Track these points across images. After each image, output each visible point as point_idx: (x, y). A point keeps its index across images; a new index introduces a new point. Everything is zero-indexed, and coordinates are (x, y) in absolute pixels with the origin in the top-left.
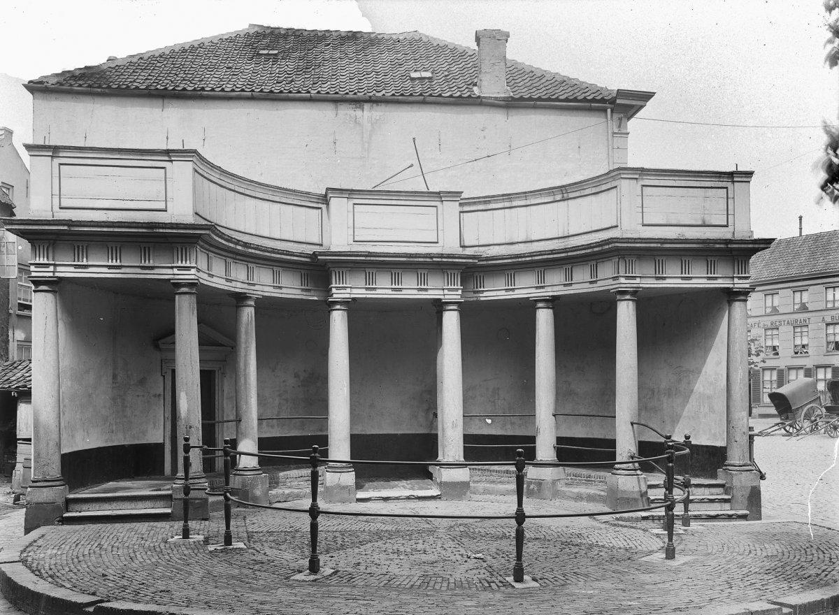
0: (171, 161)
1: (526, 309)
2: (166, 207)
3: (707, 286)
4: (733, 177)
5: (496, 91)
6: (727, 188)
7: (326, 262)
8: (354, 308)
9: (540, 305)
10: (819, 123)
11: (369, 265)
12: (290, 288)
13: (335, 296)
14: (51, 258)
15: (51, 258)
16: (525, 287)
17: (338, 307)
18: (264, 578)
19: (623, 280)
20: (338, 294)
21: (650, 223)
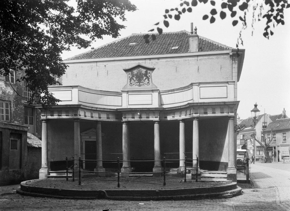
0: (73, 89)
1: (177, 123)
2: (72, 100)
3: (91, 119)
4: (228, 83)
5: (108, 65)
6: (227, 86)
7: (120, 112)
8: (128, 123)
9: (180, 121)
10: (155, 67)
11: (133, 112)
12: (112, 119)
13: (123, 120)
14: (45, 114)
15: (45, 114)
16: (177, 117)
17: (156, 123)
18: (222, 184)
19: (194, 115)
20: (124, 120)
21: (214, 97)
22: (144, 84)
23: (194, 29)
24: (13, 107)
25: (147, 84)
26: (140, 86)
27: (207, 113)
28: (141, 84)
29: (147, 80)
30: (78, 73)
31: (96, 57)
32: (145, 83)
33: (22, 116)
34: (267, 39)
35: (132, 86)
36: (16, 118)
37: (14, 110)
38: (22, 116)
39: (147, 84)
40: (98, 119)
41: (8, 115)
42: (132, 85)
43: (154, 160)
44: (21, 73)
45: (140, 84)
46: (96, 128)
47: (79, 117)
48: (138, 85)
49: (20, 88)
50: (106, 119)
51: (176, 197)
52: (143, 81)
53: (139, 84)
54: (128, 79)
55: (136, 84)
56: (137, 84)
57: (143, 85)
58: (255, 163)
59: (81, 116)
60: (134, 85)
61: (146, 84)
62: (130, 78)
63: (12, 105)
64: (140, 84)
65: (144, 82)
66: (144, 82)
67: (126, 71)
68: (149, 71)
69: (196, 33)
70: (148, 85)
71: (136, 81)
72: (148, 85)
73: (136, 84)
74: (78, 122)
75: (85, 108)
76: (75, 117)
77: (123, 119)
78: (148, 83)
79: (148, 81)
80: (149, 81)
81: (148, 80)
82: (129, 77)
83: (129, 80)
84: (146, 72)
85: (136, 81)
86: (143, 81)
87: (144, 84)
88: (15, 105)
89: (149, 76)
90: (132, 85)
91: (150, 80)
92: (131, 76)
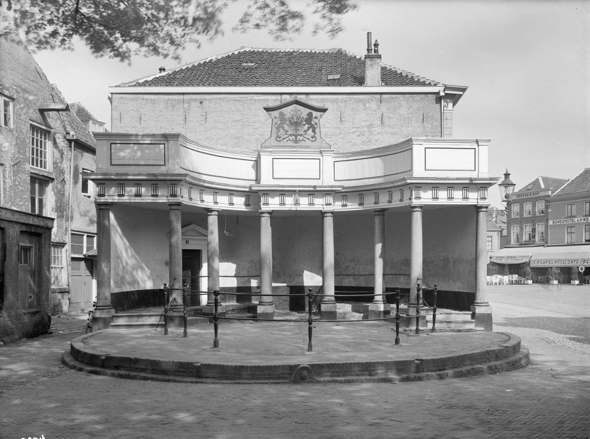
2: (428, 170)
12: (239, 204)
22: (304, 138)
23: (373, 43)
24: (9, 176)
25: (311, 139)
26: (296, 143)
27: (141, 195)
28: (298, 139)
29: (310, 131)
30: (145, 114)
31: (181, 84)
32: (308, 137)
33: (25, 196)
34: (68, 52)
35: (280, 141)
36: (15, 199)
37: (10, 184)
38: (25, 196)
39: (311, 139)
40: (294, 208)
41: (39, 196)
42: (281, 139)
43: (373, 293)
44: (24, 107)
45: (296, 138)
46: (204, 224)
47: (178, 199)
48: (293, 141)
49: (23, 138)
50: (278, 206)
51: (376, 378)
52: (303, 134)
53: (294, 139)
54: (273, 127)
55: (288, 139)
56: (291, 138)
57: (303, 140)
58: (487, 301)
59: (183, 199)
60: (284, 139)
61: (308, 139)
62: (276, 126)
63: (7, 172)
64: (296, 138)
65: (306, 134)
66: (305, 136)
67: (268, 109)
68: (315, 114)
69: (376, 51)
70: (312, 141)
71: (288, 132)
72: (312, 141)
73: (288, 139)
74: (179, 209)
75: (194, 183)
76: (173, 200)
77: (262, 206)
78: (313, 137)
79: (313, 134)
80: (315, 133)
81: (314, 131)
82: (276, 124)
83: (274, 130)
84: (310, 115)
85: (288, 132)
86: (303, 134)
87: (304, 138)
88: (12, 172)
89: (316, 124)
90: (281, 139)
91: (317, 130)
92: (279, 122)
